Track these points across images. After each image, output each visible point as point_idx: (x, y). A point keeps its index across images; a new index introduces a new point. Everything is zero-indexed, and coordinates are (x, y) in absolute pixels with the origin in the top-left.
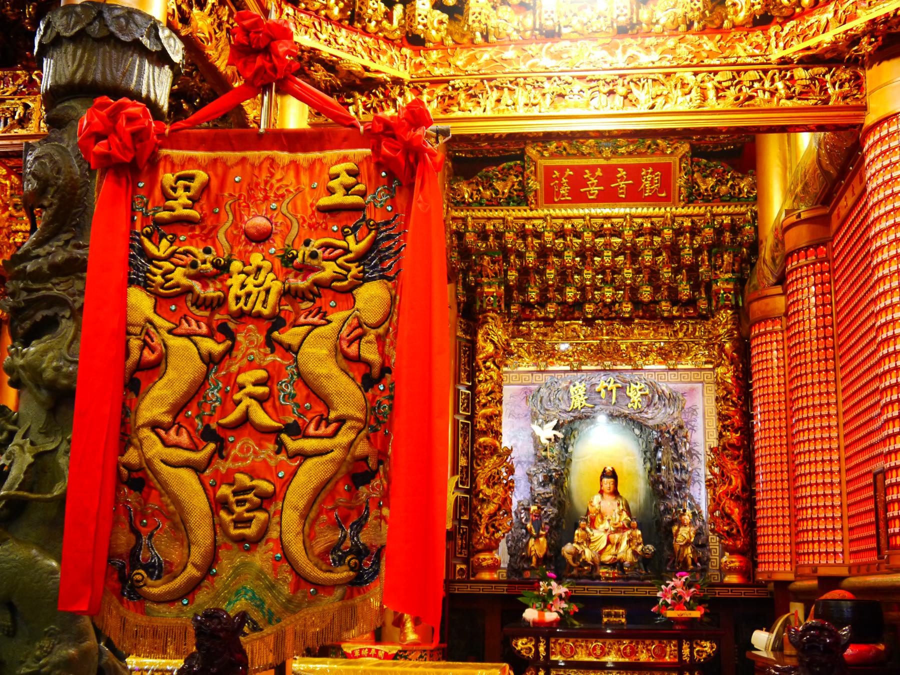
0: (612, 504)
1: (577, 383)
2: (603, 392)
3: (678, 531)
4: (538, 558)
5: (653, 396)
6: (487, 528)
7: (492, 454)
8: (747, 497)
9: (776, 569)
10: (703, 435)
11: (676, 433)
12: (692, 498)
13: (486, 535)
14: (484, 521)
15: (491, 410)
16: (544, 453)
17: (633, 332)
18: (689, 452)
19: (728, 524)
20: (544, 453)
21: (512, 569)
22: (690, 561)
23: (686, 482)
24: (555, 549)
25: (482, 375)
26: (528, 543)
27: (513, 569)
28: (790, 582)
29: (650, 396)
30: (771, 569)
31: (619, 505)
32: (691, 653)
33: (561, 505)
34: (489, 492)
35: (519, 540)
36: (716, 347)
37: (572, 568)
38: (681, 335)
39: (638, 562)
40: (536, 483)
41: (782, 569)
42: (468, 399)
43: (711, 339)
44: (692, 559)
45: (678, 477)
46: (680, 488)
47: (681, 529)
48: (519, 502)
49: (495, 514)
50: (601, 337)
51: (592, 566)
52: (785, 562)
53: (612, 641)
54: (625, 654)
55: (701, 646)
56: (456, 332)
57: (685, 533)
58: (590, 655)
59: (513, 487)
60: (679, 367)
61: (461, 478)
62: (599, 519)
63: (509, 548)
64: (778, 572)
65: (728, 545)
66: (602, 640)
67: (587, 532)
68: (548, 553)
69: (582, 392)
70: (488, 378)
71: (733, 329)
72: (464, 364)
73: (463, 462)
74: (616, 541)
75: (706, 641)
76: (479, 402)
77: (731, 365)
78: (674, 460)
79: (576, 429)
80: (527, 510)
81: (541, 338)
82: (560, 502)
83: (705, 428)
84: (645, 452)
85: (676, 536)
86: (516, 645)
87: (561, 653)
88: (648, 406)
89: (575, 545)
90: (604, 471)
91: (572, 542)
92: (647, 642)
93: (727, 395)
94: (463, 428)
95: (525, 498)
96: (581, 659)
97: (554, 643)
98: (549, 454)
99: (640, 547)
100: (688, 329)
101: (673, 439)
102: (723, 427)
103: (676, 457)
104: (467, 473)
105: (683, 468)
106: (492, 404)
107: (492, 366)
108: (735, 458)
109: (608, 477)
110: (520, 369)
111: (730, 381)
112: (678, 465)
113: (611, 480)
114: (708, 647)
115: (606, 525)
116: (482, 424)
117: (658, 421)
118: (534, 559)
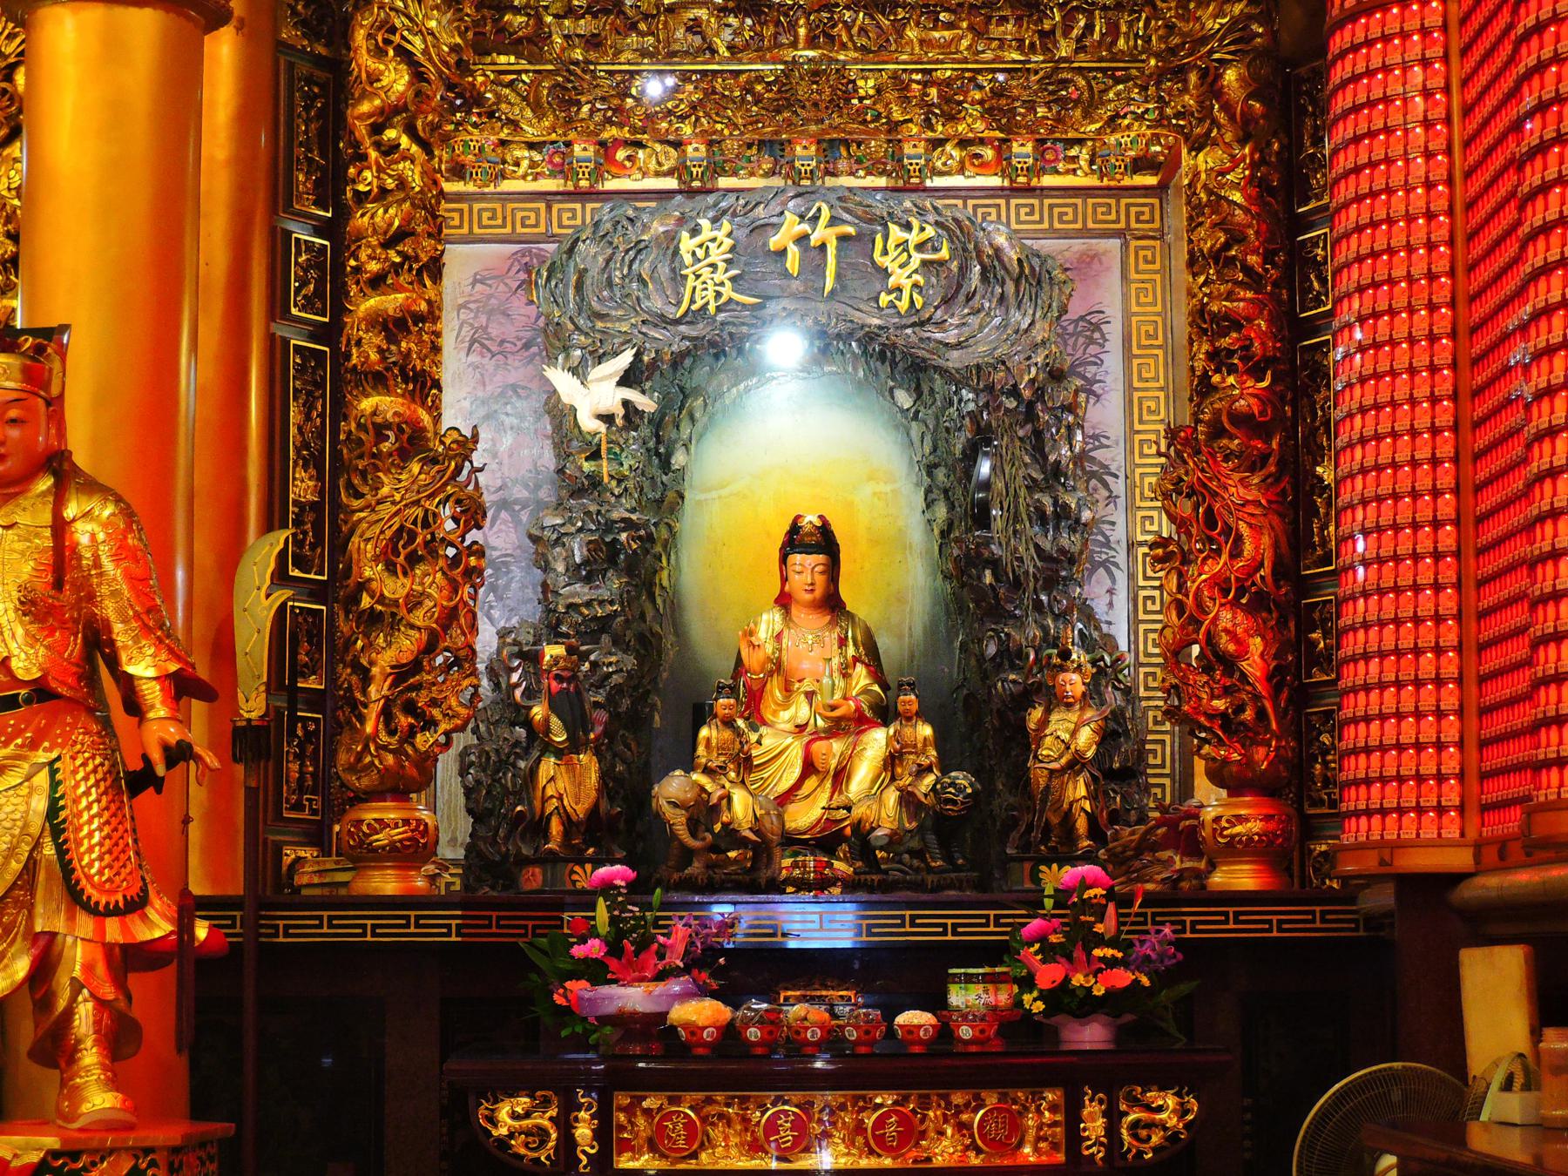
0: (819, 640)
1: (705, 223)
2: (793, 261)
3: (1044, 723)
4: (568, 822)
5: (964, 270)
6: (386, 714)
7: (404, 455)
8: (1295, 596)
9: (1409, 833)
10: (1126, 417)
11: (1039, 393)
12: (1088, 616)
13: (384, 738)
14: (377, 691)
15: (401, 296)
16: (588, 467)
17: (900, 34)
18: (1080, 458)
19: (1226, 692)
20: (588, 467)
21: (478, 861)
22: (1081, 824)
23: (1072, 561)
24: (627, 797)
25: (367, 174)
26: (533, 772)
27: (481, 862)
28: (1456, 879)
29: (954, 266)
30: (1391, 835)
31: (842, 642)
32: (1112, 1130)
33: (647, 646)
34: (395, 588)
35: (504, 764)
36: (1193, 78)
37: (688, 855)
38: (1065, 49)
39: (920, 828)
40: (561, 568)
41: (1429, 833)
42: (320, 267)
43: (1173, 51)
44: (1091, 818)
45: (1046, 545)
46: (1051, 582)
47: (1054, 717)
48: (503, 634)
49: (415, 666)
50: (789, 54)
51: (755, 847)
52: (1441, 810)
53: (830, 1096)
54: (880, 1140)
55: (1148, 1108)
56: (276, 30)
57: (1069, 732)
58: (755, 1148)
59: (479, 571)
60: (1048, 180)
61: (299, 543)
62: (775, 690)
63: (468, 792)
64: (1418, 843)
65: (1226, 761)
66: (796, 1096)
67: (738, 733)
68: (604, 805)
69: (717, 255)
70: (390, 183)
71: (1250, 18)
72: (307, 145)
73: (302, 486)
74: (833, 763)
75: (1163, 1088)
76: (357, 270)
77: (1242, 142)
78: (1033, 485)
79: (697, 391)
80: (531, 658)
81: (578, 54)
82: (642, 638)
83: (1129, 389)
84: (930, 469)
85: (1039, 740)
86: (493, 1121)
87: (653, 1146)
88: (947, 301)
89: (697, 777)
90: (795, 528)
91: (689, 766)
92: (958, 1099)
93: (1227, 246)
94: (301, 370)
95: (523, 622)
96: (723, 1165)
97: (629, 1110)
98: (605, 467)
99: (930, 779)
100: (1089, 28)
101: (1030, 415)
102: (1212, 356)
103: (1038, 476)
104: (318, 527)
105: (1062, 512)
106: (404, 279)
107: (405, 141)
108: (1254, 464)
109: (808, 549)
110: (507, 186)
111: (1237, 197)
112: (1047, 501)
113: (816, 560)
114: (1168, 1109)
115: (801, 711)
116: (368, 349)
117: (979, 352)
118: (555, 827)
